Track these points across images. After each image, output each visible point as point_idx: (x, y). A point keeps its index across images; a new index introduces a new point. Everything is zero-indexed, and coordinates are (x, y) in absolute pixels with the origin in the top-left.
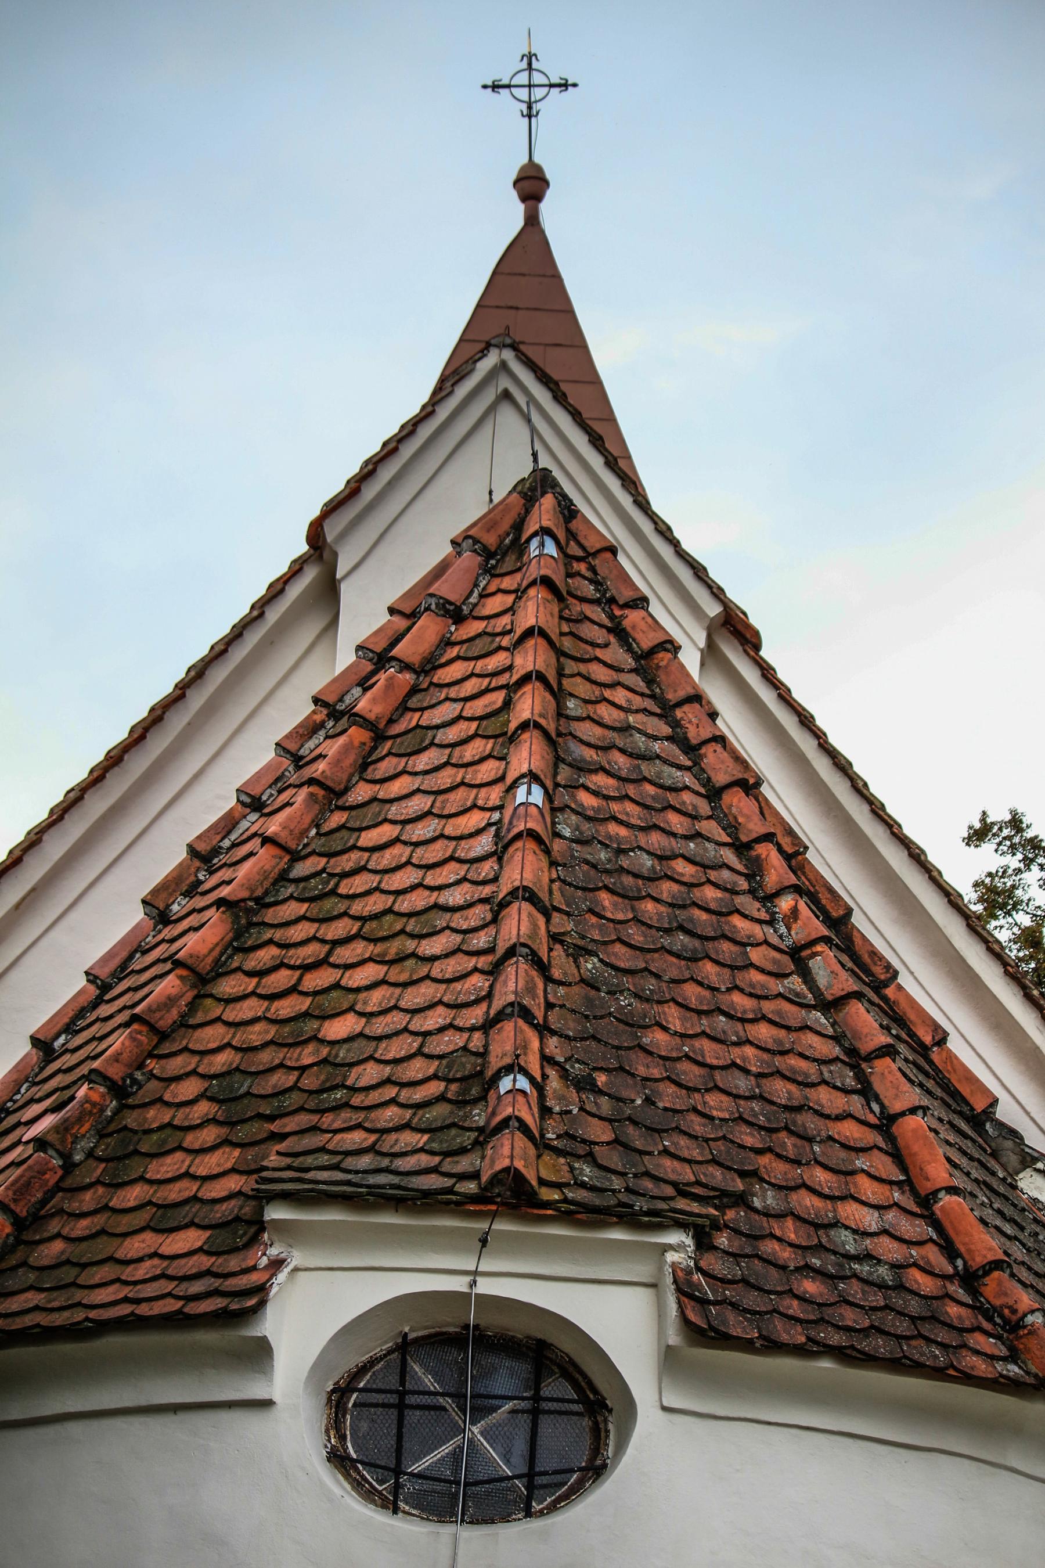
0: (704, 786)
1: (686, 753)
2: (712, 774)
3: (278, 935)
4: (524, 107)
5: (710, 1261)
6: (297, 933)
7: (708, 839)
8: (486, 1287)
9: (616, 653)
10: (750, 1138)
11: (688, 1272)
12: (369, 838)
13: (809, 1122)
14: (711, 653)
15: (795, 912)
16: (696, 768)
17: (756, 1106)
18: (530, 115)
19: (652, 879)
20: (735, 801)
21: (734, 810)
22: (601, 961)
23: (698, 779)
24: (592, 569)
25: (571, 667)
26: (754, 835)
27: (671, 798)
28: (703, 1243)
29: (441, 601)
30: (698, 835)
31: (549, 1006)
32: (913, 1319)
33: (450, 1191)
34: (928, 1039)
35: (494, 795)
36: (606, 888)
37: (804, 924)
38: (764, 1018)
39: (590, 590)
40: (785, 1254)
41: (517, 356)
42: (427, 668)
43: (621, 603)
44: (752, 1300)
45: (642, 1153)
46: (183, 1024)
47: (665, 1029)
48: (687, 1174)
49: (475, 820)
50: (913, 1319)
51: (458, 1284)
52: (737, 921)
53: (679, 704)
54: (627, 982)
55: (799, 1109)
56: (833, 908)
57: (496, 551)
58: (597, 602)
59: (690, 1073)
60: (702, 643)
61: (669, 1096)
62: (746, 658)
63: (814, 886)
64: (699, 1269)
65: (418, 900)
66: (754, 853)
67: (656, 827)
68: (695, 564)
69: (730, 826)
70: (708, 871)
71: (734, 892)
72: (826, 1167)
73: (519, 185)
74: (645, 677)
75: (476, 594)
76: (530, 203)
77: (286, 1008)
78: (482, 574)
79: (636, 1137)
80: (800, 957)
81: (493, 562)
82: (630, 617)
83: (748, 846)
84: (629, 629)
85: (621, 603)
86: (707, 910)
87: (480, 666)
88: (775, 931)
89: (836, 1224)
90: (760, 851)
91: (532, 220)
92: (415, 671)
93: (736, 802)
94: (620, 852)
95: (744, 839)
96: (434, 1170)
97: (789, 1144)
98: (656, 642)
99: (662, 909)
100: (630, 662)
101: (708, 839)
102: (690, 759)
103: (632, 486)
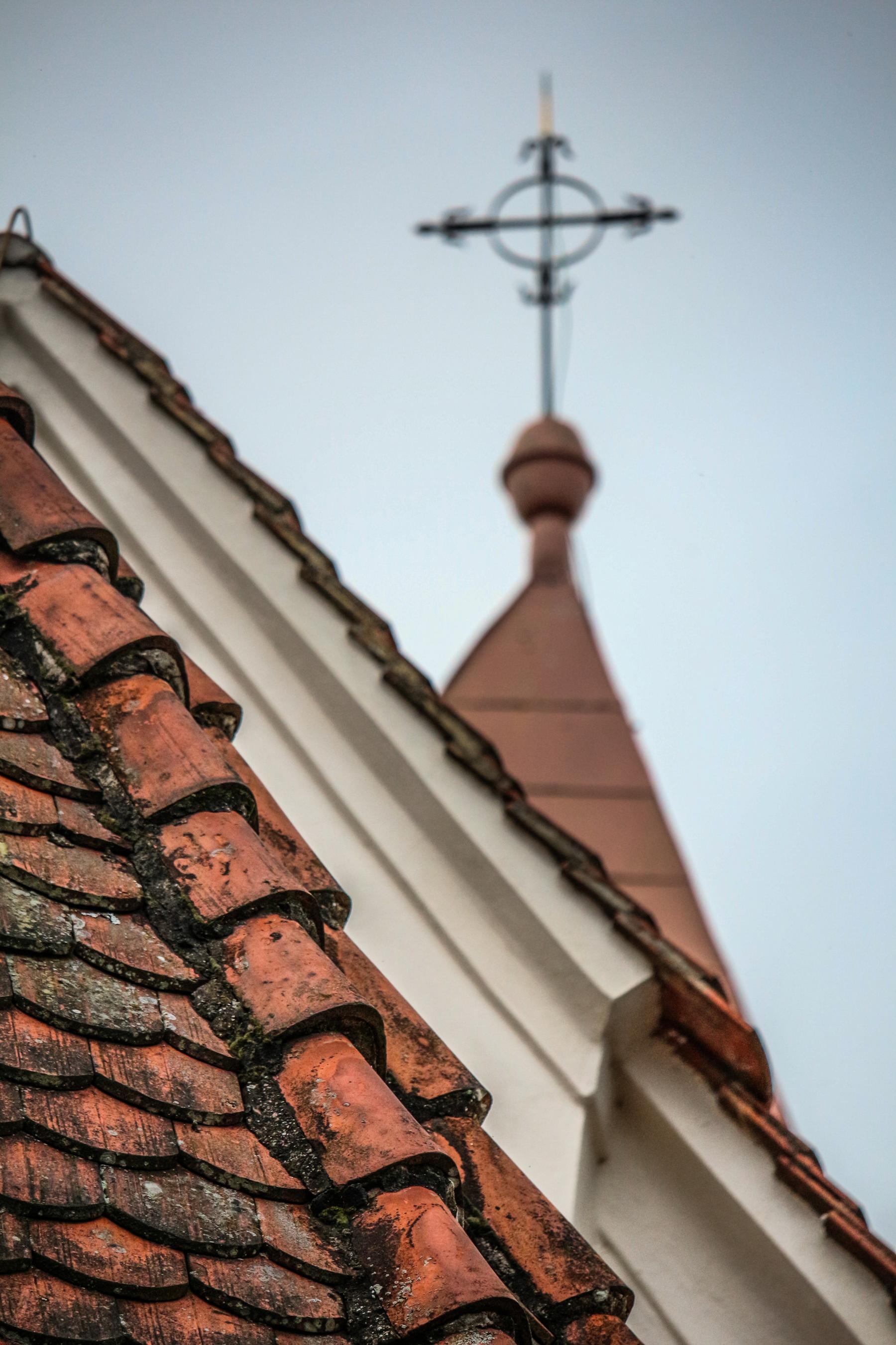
0: (226, 1036)
1: (180, 947)
2: (253, 996)
4: (530, 279)
7: (217, 1177)
14: (618, 1123)
16: (208, 988)
20: (325, 1071)
21: (317, 1097)
23: (210, 1019)
26: (376, 1163)
27: (105, 1061)
41: (44, 290)
43: (16, 544)
53: (173, 813)
62: (730, 1129)
66: (370, 1218)
70: (197, 1261)
73: (519, 476)
74: (74, 746)
76: (547, 524)
82: (43, 586)
83: (355, 1196)
84: (37, 618)
85: (16, 544)
90: (391, 1209)
91: (551, 569)
93: (333, 1080)
95: (339, 1173)
98: (117, 642)
101: (217, 1177)
102: (189, 963)
103: (378, 635)
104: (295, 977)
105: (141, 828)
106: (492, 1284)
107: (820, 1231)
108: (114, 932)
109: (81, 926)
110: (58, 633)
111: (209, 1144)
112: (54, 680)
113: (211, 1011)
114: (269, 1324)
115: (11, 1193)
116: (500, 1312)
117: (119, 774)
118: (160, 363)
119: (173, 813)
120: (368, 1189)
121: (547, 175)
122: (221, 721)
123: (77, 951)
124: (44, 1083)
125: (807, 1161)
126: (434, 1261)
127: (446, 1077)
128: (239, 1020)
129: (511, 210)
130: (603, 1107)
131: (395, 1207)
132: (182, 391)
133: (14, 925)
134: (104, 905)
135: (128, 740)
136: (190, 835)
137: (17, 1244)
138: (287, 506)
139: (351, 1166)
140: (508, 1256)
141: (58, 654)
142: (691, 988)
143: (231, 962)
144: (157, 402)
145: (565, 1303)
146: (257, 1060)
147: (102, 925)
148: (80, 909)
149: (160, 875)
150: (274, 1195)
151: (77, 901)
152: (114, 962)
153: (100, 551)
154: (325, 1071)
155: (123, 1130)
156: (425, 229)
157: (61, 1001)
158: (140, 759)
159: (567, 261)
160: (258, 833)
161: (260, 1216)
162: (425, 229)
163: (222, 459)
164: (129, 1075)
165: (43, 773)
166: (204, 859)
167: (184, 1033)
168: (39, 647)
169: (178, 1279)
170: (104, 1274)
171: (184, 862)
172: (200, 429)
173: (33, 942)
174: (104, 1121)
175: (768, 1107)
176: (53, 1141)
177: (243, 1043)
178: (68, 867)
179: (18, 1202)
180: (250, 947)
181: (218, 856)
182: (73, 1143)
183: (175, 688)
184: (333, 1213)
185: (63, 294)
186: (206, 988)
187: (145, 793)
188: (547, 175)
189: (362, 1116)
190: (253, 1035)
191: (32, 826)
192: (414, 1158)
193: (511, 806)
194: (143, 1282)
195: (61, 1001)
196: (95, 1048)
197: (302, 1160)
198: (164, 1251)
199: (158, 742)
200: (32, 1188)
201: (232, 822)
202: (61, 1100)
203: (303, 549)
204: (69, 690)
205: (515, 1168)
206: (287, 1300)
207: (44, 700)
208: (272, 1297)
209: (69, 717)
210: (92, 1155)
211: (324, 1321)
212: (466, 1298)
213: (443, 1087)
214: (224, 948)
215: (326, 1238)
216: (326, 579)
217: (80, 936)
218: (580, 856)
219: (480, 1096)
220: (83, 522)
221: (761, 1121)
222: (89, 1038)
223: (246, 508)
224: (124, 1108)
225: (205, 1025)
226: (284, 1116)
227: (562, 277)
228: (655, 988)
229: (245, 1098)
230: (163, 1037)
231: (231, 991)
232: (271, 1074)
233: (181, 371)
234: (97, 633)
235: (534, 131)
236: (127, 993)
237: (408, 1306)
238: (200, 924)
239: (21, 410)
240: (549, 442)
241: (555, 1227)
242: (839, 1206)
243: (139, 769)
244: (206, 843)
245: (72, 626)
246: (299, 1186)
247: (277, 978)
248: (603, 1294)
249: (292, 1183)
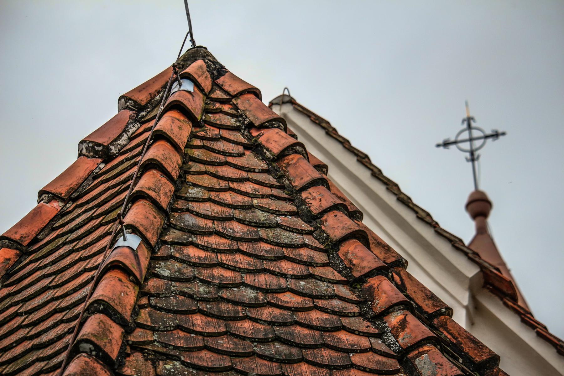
0: (323, 243)
1: (309, 222)
4: (468, 155)
7: (321, 279)
14: (476, 310)
15: (403, 324)
18: (473, 158)
19: (256, 305)
20: (351, 249)
21: (350, 256)
22: (183, 363)
23: (318, 240)
24: (236, 108)
26: (367, 270)
27: (286, 252)
29: (91, 145)
30: (311, 276)
37: (412, 331)
42: (75, 195)
43: (257, 124)
53: (304, 188)
56: (476, 354)
57: (146, 104)
58: (236, 129)
60: (466, 302)
62: (507, 310)
63: (456, 339)
66: (366, 285)
68: (452, 238)
69: (346, 268)
74: (276, 175)
75: (125, 137)
76: (480, 219)
78: (132, 123)
80: (407, 358)
81: (144, 113)
83: (362, 280)
84: (264, 143)
85: (257, 124)
88: (384, 342)
90: (372, 282)
92: (62, 200)
93: (353, 251)
95: (356, 274)
98: (286, 146)
101: (321, 279)
102: (311, 226)
103: (394, 188)
104: (341, 225)
105: (296, 193)
106: (401, 297)
107: (535, 334)
108: (289, 220)
109: (279, 219)
110: (269, 146)
111: (318, 271)
112: (269, 158)
113: (318, 237)
114: (338, 315)
115: (260, 286)
116: (406, 305)
117: (289, 180)
118: (328, 123)
119: (304, 188)
120: (366, 277)
121: (469, 127)
122: (322, 170)
123: (278, 226)
124: (270, 258)
125: (529, 316)
126: (385, 294)
127: (393, 257)
128: (326, 239)
129: (461, 138)
130: (471, 309)
131: (373, 281)
132: (334, 129)
133: (260, 220)
134: (286, 213)
135: (291, 171)
136: (310, 193)
137: (262, 299)
138: (366, 156)
139: (360, 272)
140: (415, 302)
141: (270, 151)
142: (491, 272)
143: (323, 224)
144: (328, 134)
145: (432, 313)
146: (332, 248)
147: (286, 219)
148: (279, 215)
149: (302, 205)
150: (338, 282)
151: (278, 213)
152: (289, 227)
153: (281, 124)
154: (351, 249)
155: (293, 269)
156: (438, 146)
157: (274, 238)
158: (294, 175)
159: (477, 149)
160: (369, 248)
161: (335, 288)
162: (438, 146)
163: (347, 146)
164: (294, 255)
165: (267, 182)
166: (314, 198)
167: (311, 244)
168: (265, 150)
169: (311, 305)
170: (289, 305)
171: (308, 200)
172: (340, 139)
173: (265, 224)
174: (287, 267)
175: (517, 302)
176: (273, 273)
177: (327, 245)
178: (274, 205)
179: (262, 288)
180: (328, 219)
181: (318, 197)
182: (278, 273)
183: (305, 157)
184: (356, 285)
185: (299, 108)
186: (316, 232)
187: (296, 184)
188: (469, 127)
189: (362, 259)
190: (330, 242)
191: (264, 195)
192: (378, 267)
193: (436, 229)
194: (300, 306)
195: (274, 238)
196: (284, 249)
197: (346, 273)
198: (306, 298)
199: (299, 170)
200: (266, 285)
201: (322, 189)
202: (275, 263)
203: (372, 167)
204: (274, 160)
205: (416, 279)
206: (343, 308)
207: (267, 164)
208: (339, 308)
209: (274, 167)
210: (284, 276)
211: (354, 313)
212: (395, 301)
213: (393, 259)
214: (321, 221)
215: (354, 292)
216: (379, 175)
217: (279, 222)
218: (457, 240)
219: (404, 261)
220: (275, 116)
221: (515, 307)
222: (283, 247)
223: (355, 159)
224: (293, 264)
225: (317, 241)
226: (340, 262)
227: (476, 154)
228: (482, 274)
229: (329, 259)
230: (304, 245)
231: (324, 232)
232: (336, 252)
233: (333, 125)
234: (281, 144)
235: (465, 116)
236: (294, 235)
237: (378, 306)
238: (314, 215)
239: (257, 91)
240: (477, 196)
241: (428, 293)
242: (539, 327)
243: (294, 178)
244: (314, 194)
245: (273, 143)
246: (346, 279)
247: (336, 226)
248: (444, 310)
249: (344, 279)
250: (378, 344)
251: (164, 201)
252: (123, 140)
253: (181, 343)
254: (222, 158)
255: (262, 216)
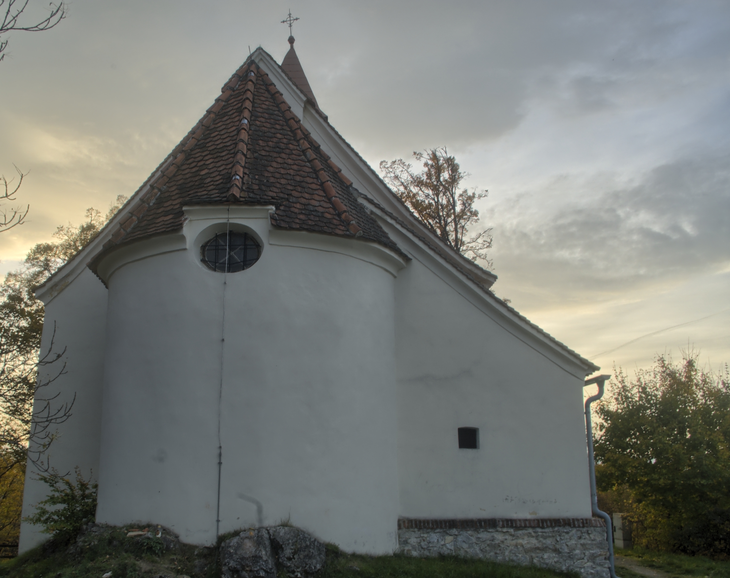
3: (194, 156)
5: (278, 212)
6: (197, 155)
8: (231, 221)
9: (267, 95)
10: (290, 187)
11: (273, 214)
12: (212, 135)
13: (304, 184)
17: (292, 181)
19: (271, 138)
25: (256, 97)
27: (277, 122)
28: (277, 208)
31: (246, 163)
32: (325, 223)
33: (221, 200)
34: (337, 171)
35: (237, 123)
36: (261, 140)
38: (295, 164)
39: (262, 83)
40: (296, 211)
44: (288, 219)
45: (265, 191)
46: (174, 176)
47: (272, 167)
48: (275, 195)
49: (234, 128)
50: (325, 223)
51: (225, 221)
52: (291, 145)
54: (265, 158)
55: (302, 182)
58: (263, 85)
59: (277, 175)
60: (303, 106)
61: (272, 180)
64: (276, 213)
65: (221, 146)
67: (273, 128)
71: (290, 140)
72: (307, 193)
77: (194, 170)
79: (263, 188)
86: (284, 144)
87: (237, 99)
89: (309, 204)
91: (292, 47)
94: (265, 133)
96: (218, 197)
97: (299, 189)
99: (274, 143)
100: (270, 96)
250: (298, 148)
251: (251, 109)
252: (237, 86)
253: (258, 149)
254: (261, 94)
255: (271, 111)
